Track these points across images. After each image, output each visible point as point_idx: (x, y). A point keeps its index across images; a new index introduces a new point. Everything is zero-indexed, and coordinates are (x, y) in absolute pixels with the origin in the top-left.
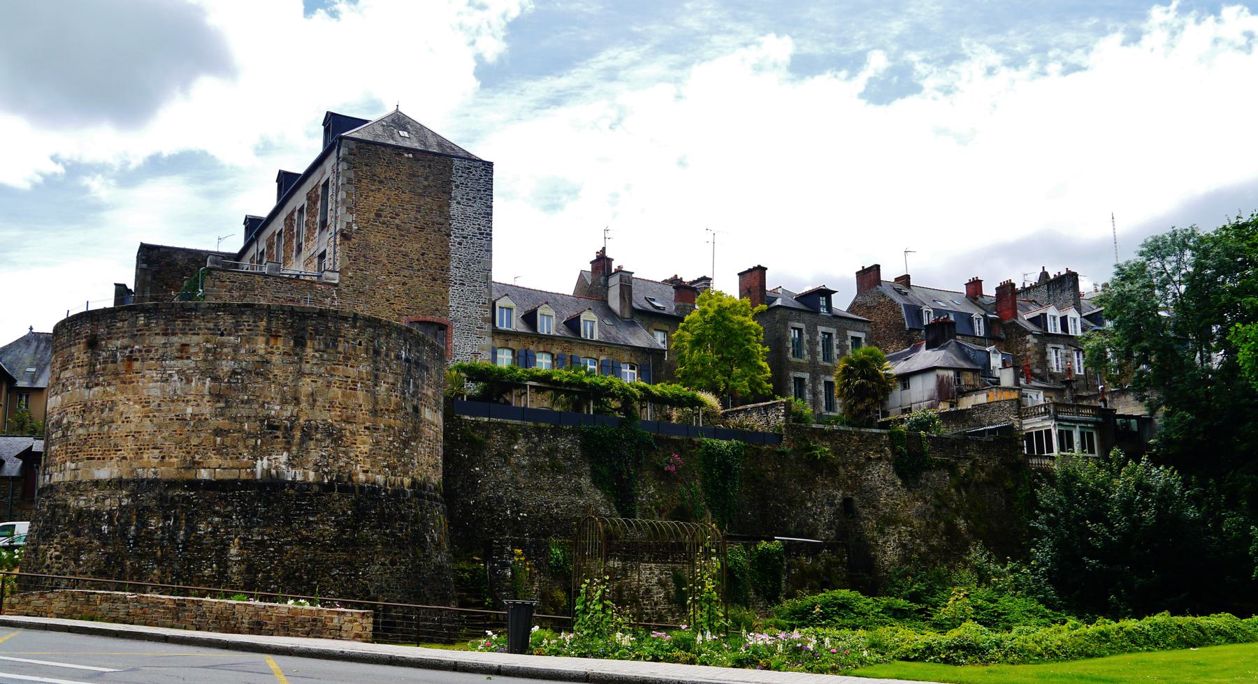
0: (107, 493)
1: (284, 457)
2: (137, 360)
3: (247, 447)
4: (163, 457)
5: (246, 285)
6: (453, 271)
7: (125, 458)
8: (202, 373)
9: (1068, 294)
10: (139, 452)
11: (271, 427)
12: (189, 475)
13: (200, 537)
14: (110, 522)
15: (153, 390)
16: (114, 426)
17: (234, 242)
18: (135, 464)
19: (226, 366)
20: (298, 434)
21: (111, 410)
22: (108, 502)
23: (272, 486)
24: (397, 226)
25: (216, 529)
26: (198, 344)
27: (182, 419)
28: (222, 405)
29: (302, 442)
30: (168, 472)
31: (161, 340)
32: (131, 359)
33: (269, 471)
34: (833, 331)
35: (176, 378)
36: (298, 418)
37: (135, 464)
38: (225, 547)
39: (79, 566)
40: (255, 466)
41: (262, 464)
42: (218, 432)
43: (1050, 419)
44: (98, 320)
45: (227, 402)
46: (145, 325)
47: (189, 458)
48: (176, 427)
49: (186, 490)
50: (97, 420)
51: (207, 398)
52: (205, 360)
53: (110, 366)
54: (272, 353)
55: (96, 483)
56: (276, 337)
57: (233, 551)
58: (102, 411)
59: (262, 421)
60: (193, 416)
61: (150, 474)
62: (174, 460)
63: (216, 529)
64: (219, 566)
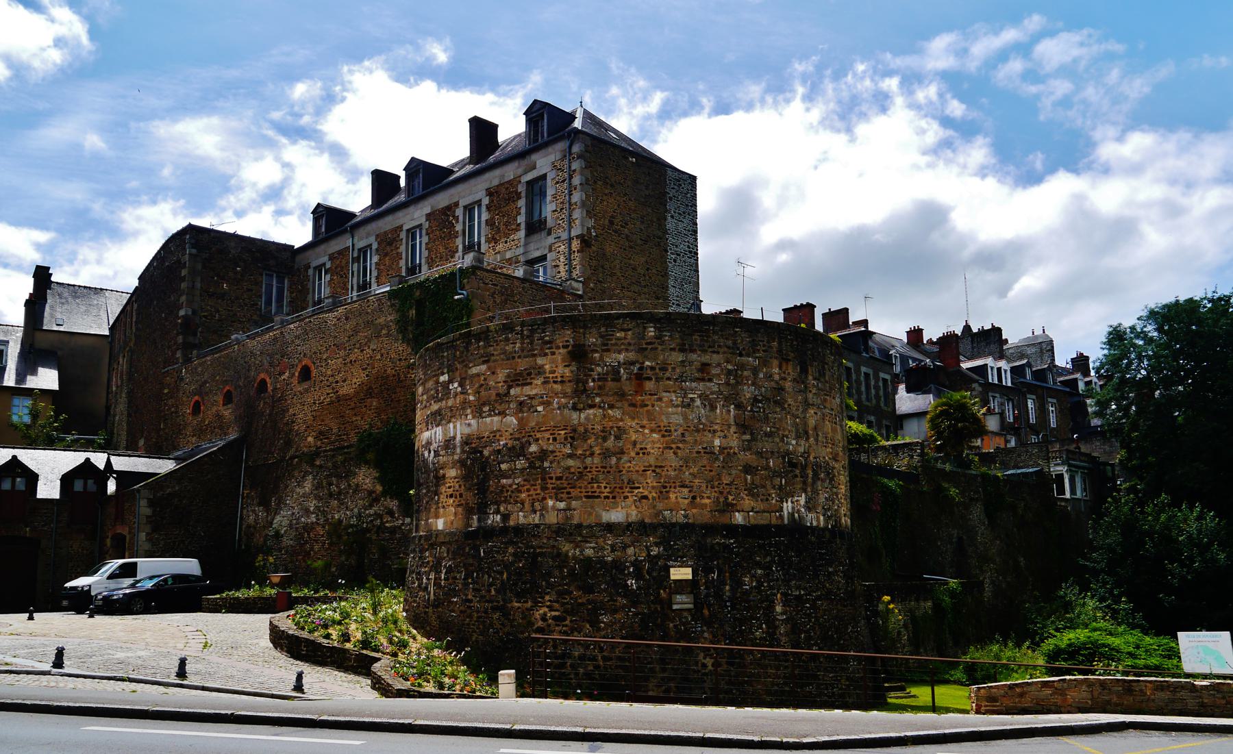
0: (627, 540)
1: (802, 500)
2: (650, 379)
3: (774, 487)
4: (694, 498)
5: (506, 289)
6: (671, 290)
7: (646, 497)
8: (726, 399)
9: (993, 347)
10: (663, 491)
11: (793, 465)
12: (724, 520)
13: (746, 593)
14: (638, 575)
15: (675, 418)
16: (625, 458)
17: (296, 232)
18: (660, 506)
19: (748, 392)
20: (810, 473)
21: (617, 438)
22: (630, 551)
23: (796, 528)
24: (627, 236)
25: (760, 584)
26: (719, 365)
27: (709, 452)
28: (748, 437)
29: (814, 483)
30: (701, 515)
31: (678, 357)
32: (640, 378)
33: (793, 514)
34: (870, 372)
35: (698, 402)
36: (808, 453)
37: (660, 506)
38: (771, 607)
39: (599, 629)
40: (781, 509)
41: (787, 506)
42: (748, 469)
43: (1063, 464)
44: (585, 327)
45: (752, 434)
46: (656, 337)
47: (722, 500)
48: (705, 462)
49: (724, 537)
50: (597, 450)
51: (733, 429)
52: (727, 384)
53: (610, 384)
54: (785, 379)
55: (610, 527)
56: (787, 361)
57: (779, 609)
58: (605, 439)
59: (784, 458)
60: (722, 449)
61: (679, 517)
62: (707, 501)
63: (760, 584)
64: (768, 627)
